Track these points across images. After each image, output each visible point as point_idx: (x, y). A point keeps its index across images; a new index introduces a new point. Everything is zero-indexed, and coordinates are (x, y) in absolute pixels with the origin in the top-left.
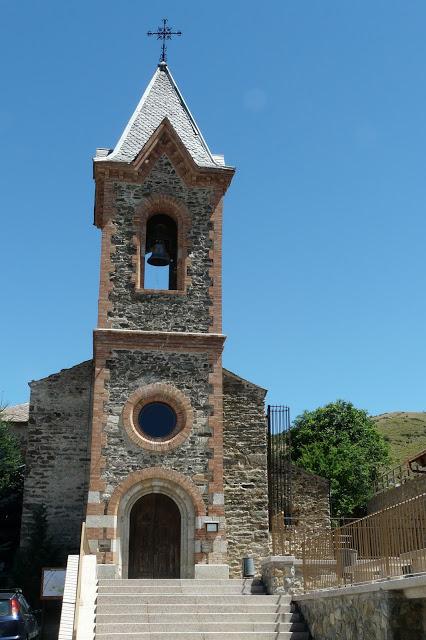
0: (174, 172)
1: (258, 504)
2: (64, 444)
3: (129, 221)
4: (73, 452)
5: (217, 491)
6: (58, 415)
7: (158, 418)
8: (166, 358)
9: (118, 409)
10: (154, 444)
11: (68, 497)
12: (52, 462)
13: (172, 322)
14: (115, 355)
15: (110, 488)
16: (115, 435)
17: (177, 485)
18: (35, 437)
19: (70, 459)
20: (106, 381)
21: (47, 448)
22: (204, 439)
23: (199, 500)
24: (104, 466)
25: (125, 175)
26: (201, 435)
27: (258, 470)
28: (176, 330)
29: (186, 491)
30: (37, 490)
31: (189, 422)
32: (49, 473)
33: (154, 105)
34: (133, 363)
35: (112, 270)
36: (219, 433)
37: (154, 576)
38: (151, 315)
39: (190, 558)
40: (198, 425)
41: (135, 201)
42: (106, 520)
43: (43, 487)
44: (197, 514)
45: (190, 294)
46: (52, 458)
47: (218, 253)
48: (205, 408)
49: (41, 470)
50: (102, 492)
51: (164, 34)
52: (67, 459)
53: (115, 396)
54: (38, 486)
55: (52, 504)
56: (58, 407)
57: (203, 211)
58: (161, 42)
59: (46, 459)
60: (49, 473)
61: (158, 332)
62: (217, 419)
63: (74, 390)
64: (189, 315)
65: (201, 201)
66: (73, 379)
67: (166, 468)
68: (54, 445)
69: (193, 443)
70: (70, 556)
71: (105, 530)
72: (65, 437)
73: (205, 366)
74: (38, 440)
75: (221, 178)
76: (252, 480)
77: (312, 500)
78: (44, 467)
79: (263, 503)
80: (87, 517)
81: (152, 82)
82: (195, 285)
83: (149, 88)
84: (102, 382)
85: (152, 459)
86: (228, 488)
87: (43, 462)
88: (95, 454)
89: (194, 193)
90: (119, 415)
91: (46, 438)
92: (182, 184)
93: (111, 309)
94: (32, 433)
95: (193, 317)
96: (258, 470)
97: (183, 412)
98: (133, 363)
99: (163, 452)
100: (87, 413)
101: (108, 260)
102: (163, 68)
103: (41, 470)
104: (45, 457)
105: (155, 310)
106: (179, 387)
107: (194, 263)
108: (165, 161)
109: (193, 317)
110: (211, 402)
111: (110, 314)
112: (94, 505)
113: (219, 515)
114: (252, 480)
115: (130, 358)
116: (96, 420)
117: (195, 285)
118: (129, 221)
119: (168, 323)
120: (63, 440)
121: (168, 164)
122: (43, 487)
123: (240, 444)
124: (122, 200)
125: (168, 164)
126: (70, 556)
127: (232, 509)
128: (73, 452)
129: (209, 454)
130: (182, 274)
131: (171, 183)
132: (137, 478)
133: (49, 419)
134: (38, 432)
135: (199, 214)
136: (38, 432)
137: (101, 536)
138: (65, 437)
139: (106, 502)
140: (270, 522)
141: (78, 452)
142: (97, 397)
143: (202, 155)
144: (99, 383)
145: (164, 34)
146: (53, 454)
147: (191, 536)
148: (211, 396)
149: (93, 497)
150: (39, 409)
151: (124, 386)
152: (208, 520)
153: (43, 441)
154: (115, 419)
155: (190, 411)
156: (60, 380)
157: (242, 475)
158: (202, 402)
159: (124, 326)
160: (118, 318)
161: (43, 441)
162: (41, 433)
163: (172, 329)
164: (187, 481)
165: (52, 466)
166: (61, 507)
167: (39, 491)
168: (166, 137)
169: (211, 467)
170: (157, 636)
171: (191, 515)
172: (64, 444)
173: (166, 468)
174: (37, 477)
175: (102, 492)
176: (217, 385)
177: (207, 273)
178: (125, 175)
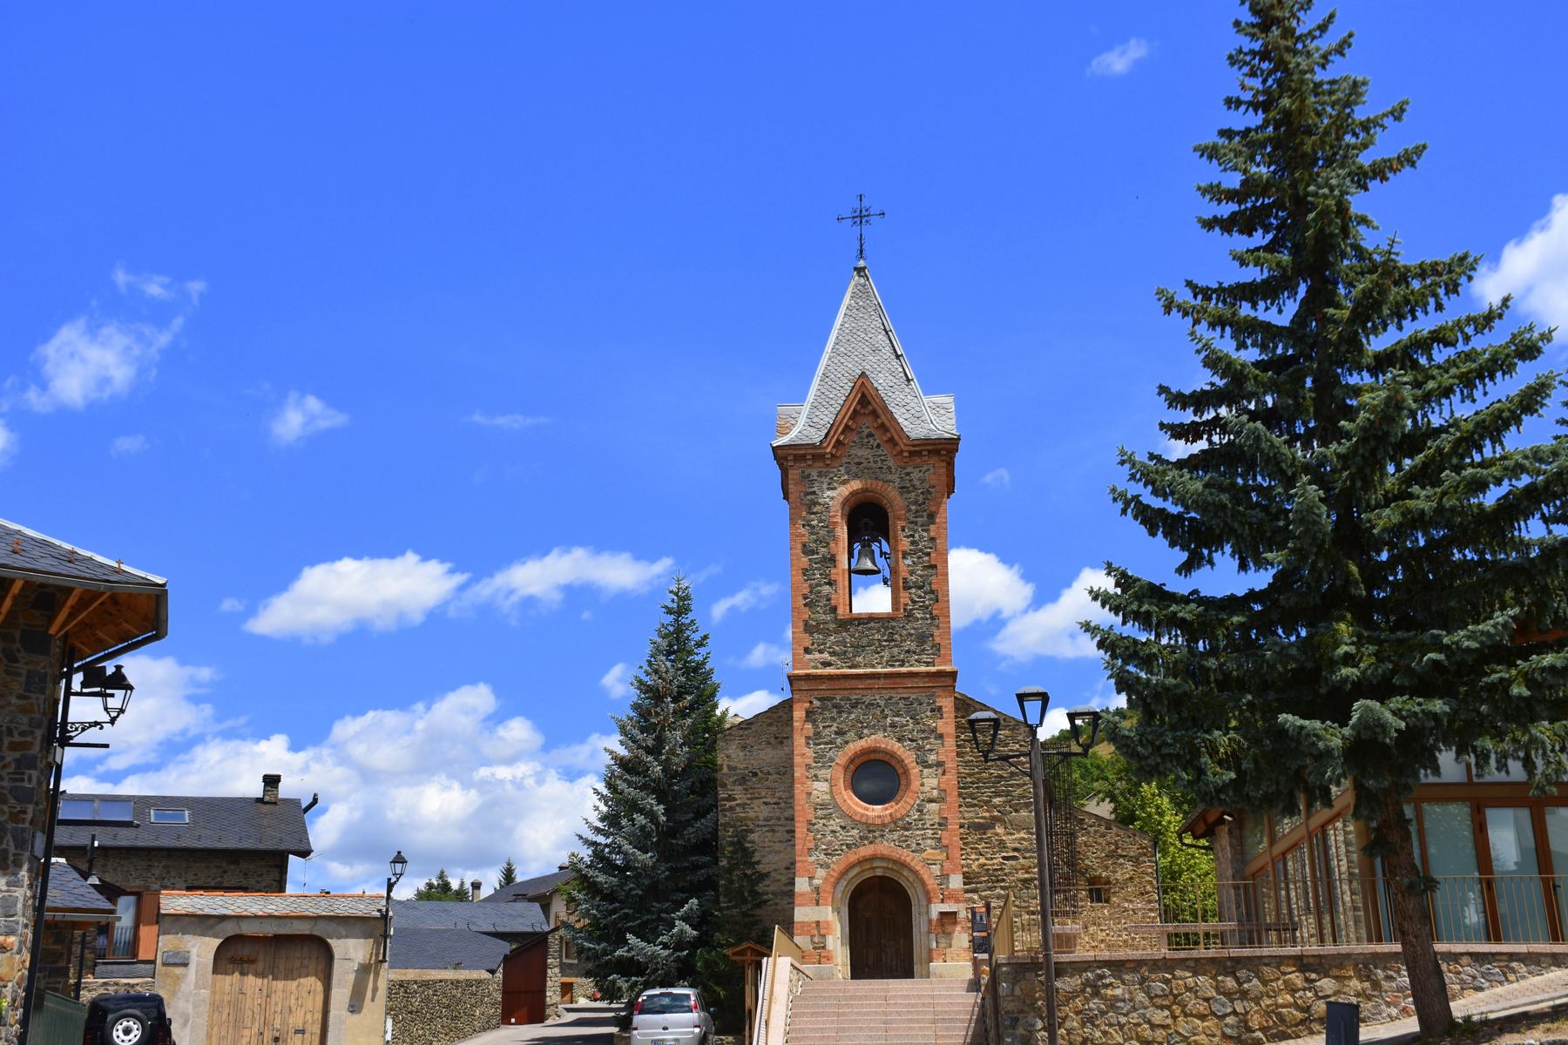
0: (878, 446)
1: (1025, 881)
2: (764, 812)
5: (953, 872)
6: (755, 774)
7: (877, 777)
8: (882, 703)
9: (823, 773)
10: (876, 811)
13: (886, 654)
15: (821, 873)
16: (823, 806)
17: (904, 865)
20: (808, 738)
23: (932, 883)
24: (812, 845)
25: (816, 457)
26: (931, 801)
27: (1022, 835)
29: (916, 873)
31: (915, 785)
33: (855, 344)
35: (806, 591)
36: (953, 797)
37: (223, 799)
38: (859, 648)
39: (924, 956)
40: (926, 789)
42: (822, 915)
44: (929, 901)
50: (811, 878)
51: (861, 217)
53: (818, 758)
57: (921, 499)
58: (857, 229)
61: (869, 670)
62: (951, 778)
63: (772, 740)
64: (909, 644)
65: (917, 483)
66: (770, 725)
68: (752, 814)
70: (1417, 1029)
71: (818, 923)
75: (944, 450)
76: (1015, 850)
77: (1129, 865)
79: (1032, 880)
81: (847, 300)
82: (914, 602)
83: (843, 309)
84: (803, 740)
85: (871, 831)
86: (982, 860)
88: (801, 829)
91: (743, 806)
92: (891, 463)
93: (808, 644)
95: (913, 646)
96: (1022, 835)
97: (906, 772)
99: (884, 825)
100: (785, 770)
101: (801, 578)
102: (860, 270)
105: (865, 641)
106: (899, 740)
107: (912, 573)
108: (867, 431)
109: (913, 646)
110: (942, 758)
111: (807, 651)
112: (802, 895)
113: (958, 901)
114: (1015, 850)
115: (835, 706)
116: (798, 789)
117: (914, 602)
121: (870, 435)
123: (997, 801)
125: (870, 435)
126: (1417, 1029)
127: (990, 889)
129: (943, 824)
132: (853, 858)
133: (743, 780)
135: (916, 503)
139: (817, 889)
140: (1043, 904)
141: (783, 822)
142: (797, 759)
143: (924, 413)
144: (799, 740)
145: (861, 217)
147: (924, 928)
148: (942, 750)
149: (801, 885)
151: (831, 743)
152: (946, 908)
154: (822, 786)
155: (915, 770)
156: (754, 727)
157: (1002, 842)
158: (932, 758)
159: (826, 664)
160: (817, 655)
163: (888, 664)
164: (914, 860)
168: (865, 407)
169: (945, 842)
171: (924, 902)
173: (885, 847)
175: (811, 878)
176: (949, 735)
178: (816, 457)
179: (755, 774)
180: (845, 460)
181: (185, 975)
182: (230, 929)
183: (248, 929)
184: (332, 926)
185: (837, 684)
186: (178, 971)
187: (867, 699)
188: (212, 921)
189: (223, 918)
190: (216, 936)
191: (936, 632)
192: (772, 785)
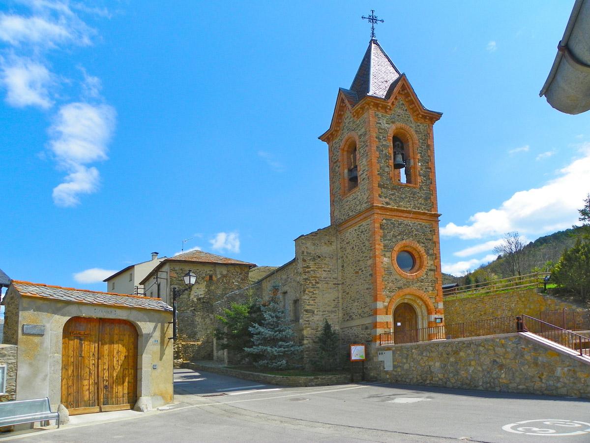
2: (324, 275)
3: (385, 137)
4: (329, 280)
5: (440, 301)
6: (319, 257)
8: (411, 225)
9: (388, 254)
11: (329, 306)
12: (318, 285)
14: (384, 221)
18: (307, 270)
19: (328, 283)
21: (315, 277)
22: (432, 273)
28: (415, 209)
30: (311, 301)
32: (317, 292)
34: (394, 227)
41: (387, 125)
43: (314, 300)
45: (421, 188)
46: (317, 283)
47: (434, 164)
48: (431, 255)
49: (312, 290)
52: (326, 283)
54: (311, 299)
55: (320, 310)
56: (318, 252)
57: (424, 138)
59: (314, 283)
60: (317, 292)
66: (326, 235)
67: (413, 289)
69: (427, 274)
70: (353, 358)
72: (324, 271)
73: (431, 231)
74: (308, 272)
78: (314, 288)
80: (20, 313)
87: (313, 285)
89: (419, 126)
90: (389, 257)
91: (314, 271)
94: (304, 267)
98: (394, 227)
103: (312, 290)
104: (314, 282)
106: (418, 242)
107: (421, 169)
108: (401, 102)
112: (380, 309)
115: (392, 223)
118: (385, 137)
119: (411, 204)
120: (323, 272)
121: (403, 104)
122: (314, 300)
124: (380, 123)
125: (403, 104)
126: (353, 358)
128: (329, 280)
130: (415, 176)
131: (405, 117)
133: (314, 259)
134: (308, 267)
135: (422, 139)
136: (308, 267)
137: (386, 326)
138: (324, 271)
141: (332, 279)
146: (318, 281)
150: (307, 253)
152: (436, 316)
153: (312, 272)
161: (312, 272)
162: (310, 268)
165: (319, 288)
166: (325, 311)
167: (312, 302)
170: (270, 374)
172: (324, 275)
173: (413, 289)
174: (310, 294)
177: (429, 176)
179: (319, 257)
180: (393, 112)
181: (42, 343)
182: (74, 311)
183: (85, 313)
184: (141, 314)
185: (394, 213)
186: (36, 339)
187: (405, 222)
188: (60, 305)
189: (68, 303)
190: (64, 315)
191: (432, 197)
192: (327, 263)
